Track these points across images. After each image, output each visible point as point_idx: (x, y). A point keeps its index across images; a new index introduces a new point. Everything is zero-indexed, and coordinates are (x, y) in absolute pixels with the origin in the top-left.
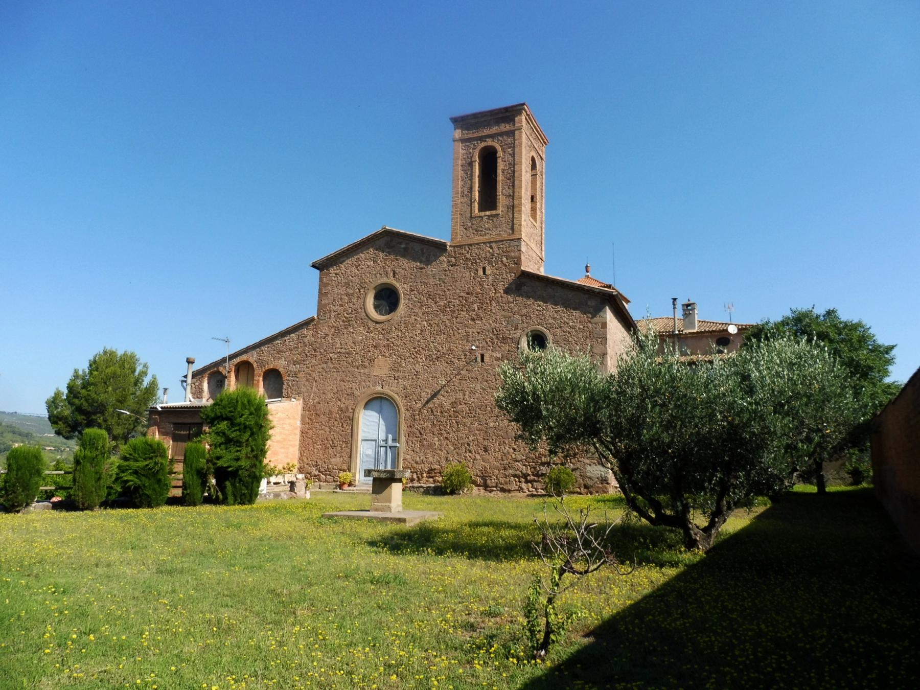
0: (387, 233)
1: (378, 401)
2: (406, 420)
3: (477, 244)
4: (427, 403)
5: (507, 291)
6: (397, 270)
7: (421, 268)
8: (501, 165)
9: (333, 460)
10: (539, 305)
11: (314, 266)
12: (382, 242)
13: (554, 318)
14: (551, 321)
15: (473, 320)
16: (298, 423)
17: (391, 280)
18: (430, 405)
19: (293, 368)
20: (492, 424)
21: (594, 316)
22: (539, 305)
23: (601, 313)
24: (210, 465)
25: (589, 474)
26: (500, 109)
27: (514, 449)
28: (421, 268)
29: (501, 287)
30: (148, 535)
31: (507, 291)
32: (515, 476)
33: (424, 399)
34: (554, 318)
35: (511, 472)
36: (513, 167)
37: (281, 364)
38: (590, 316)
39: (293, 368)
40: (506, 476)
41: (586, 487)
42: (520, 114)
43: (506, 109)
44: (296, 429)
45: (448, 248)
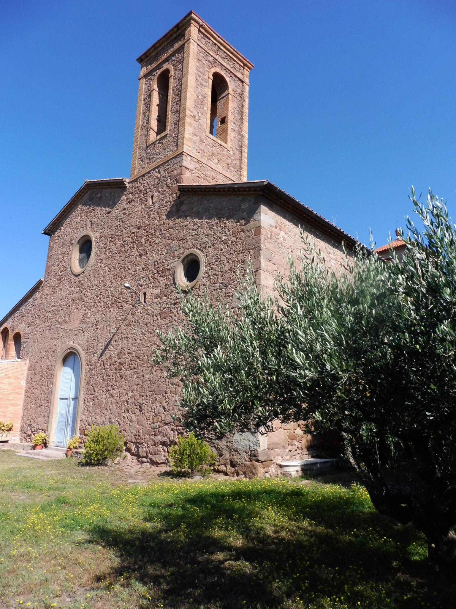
0: (90, 187)
1: (70, 357)
2: (86, 376)
3: (149, 172)
4: (101, 355)
5: (169, 216)
6: (94, 220)
7: (109, 213)
8: (172, 83)
9: (39, 419)
10: (195, 224)
11: (45, 233)
12: (86, 197)
13: (208, 235)
14: (205, 240)
15: (140, 256)
16: (23, 383)
17: (187, 252)
18: (103, 358)
19: (28, 330)
20: (147, 377)
21: (248, 222)
22: (195, 224)
23: (255, 216)
24: (188, 448)
25: (236, 446)
26: (173, 29)
27: (164, 408)
28: (109, 213)
29: (164, 212)
30: (106, 503)
31: (169, 216)
32: (163, 444)
33: (99, 352)
34: (208, 235)
35: (159, 438)
36: (181, 81)
37: (21, 328)
38: (243, 222)
39: (28, 330)
40: (155, 444)
41: (233, 465)
42: (189, 25)
43: (177, 26)
44: (21, 388)
45: (127, 185)
